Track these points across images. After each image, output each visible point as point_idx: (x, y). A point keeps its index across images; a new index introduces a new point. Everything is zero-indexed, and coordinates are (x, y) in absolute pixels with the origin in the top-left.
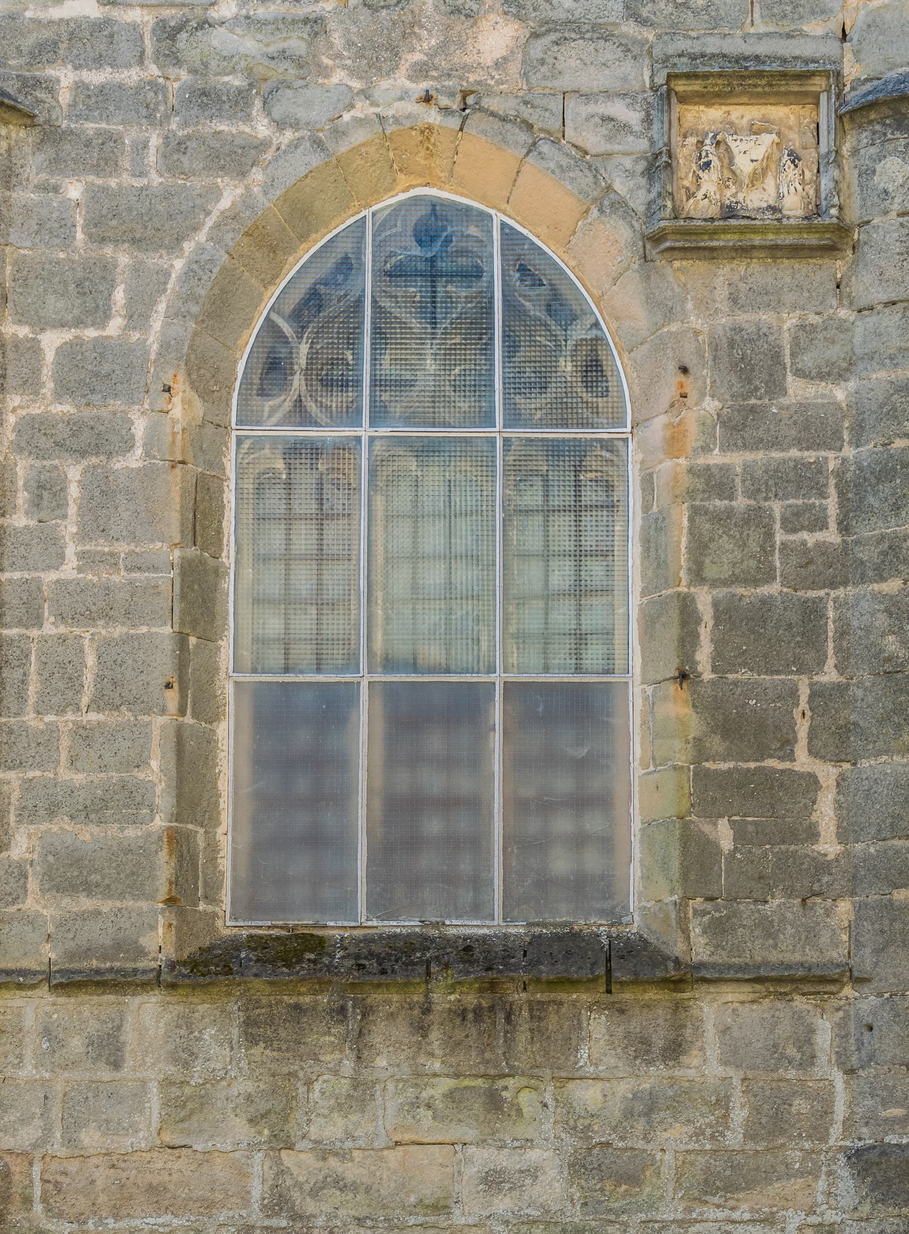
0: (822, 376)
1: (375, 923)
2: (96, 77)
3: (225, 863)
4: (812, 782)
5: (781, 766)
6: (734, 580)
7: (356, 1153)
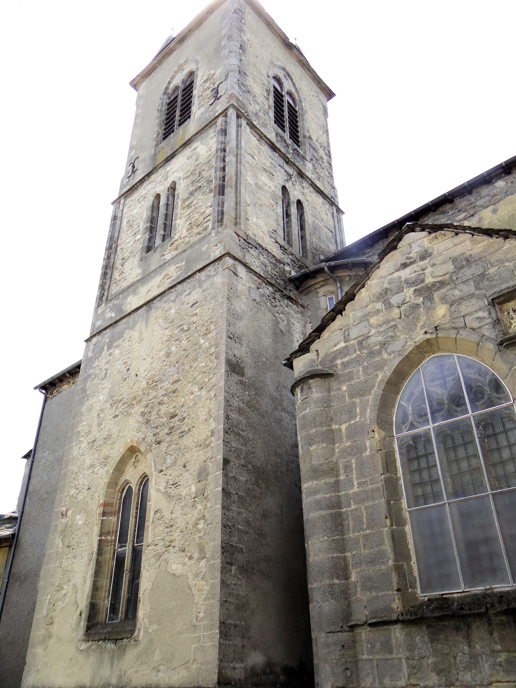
1: (468, 590)
2: (345, 360)
3: (416, 574)
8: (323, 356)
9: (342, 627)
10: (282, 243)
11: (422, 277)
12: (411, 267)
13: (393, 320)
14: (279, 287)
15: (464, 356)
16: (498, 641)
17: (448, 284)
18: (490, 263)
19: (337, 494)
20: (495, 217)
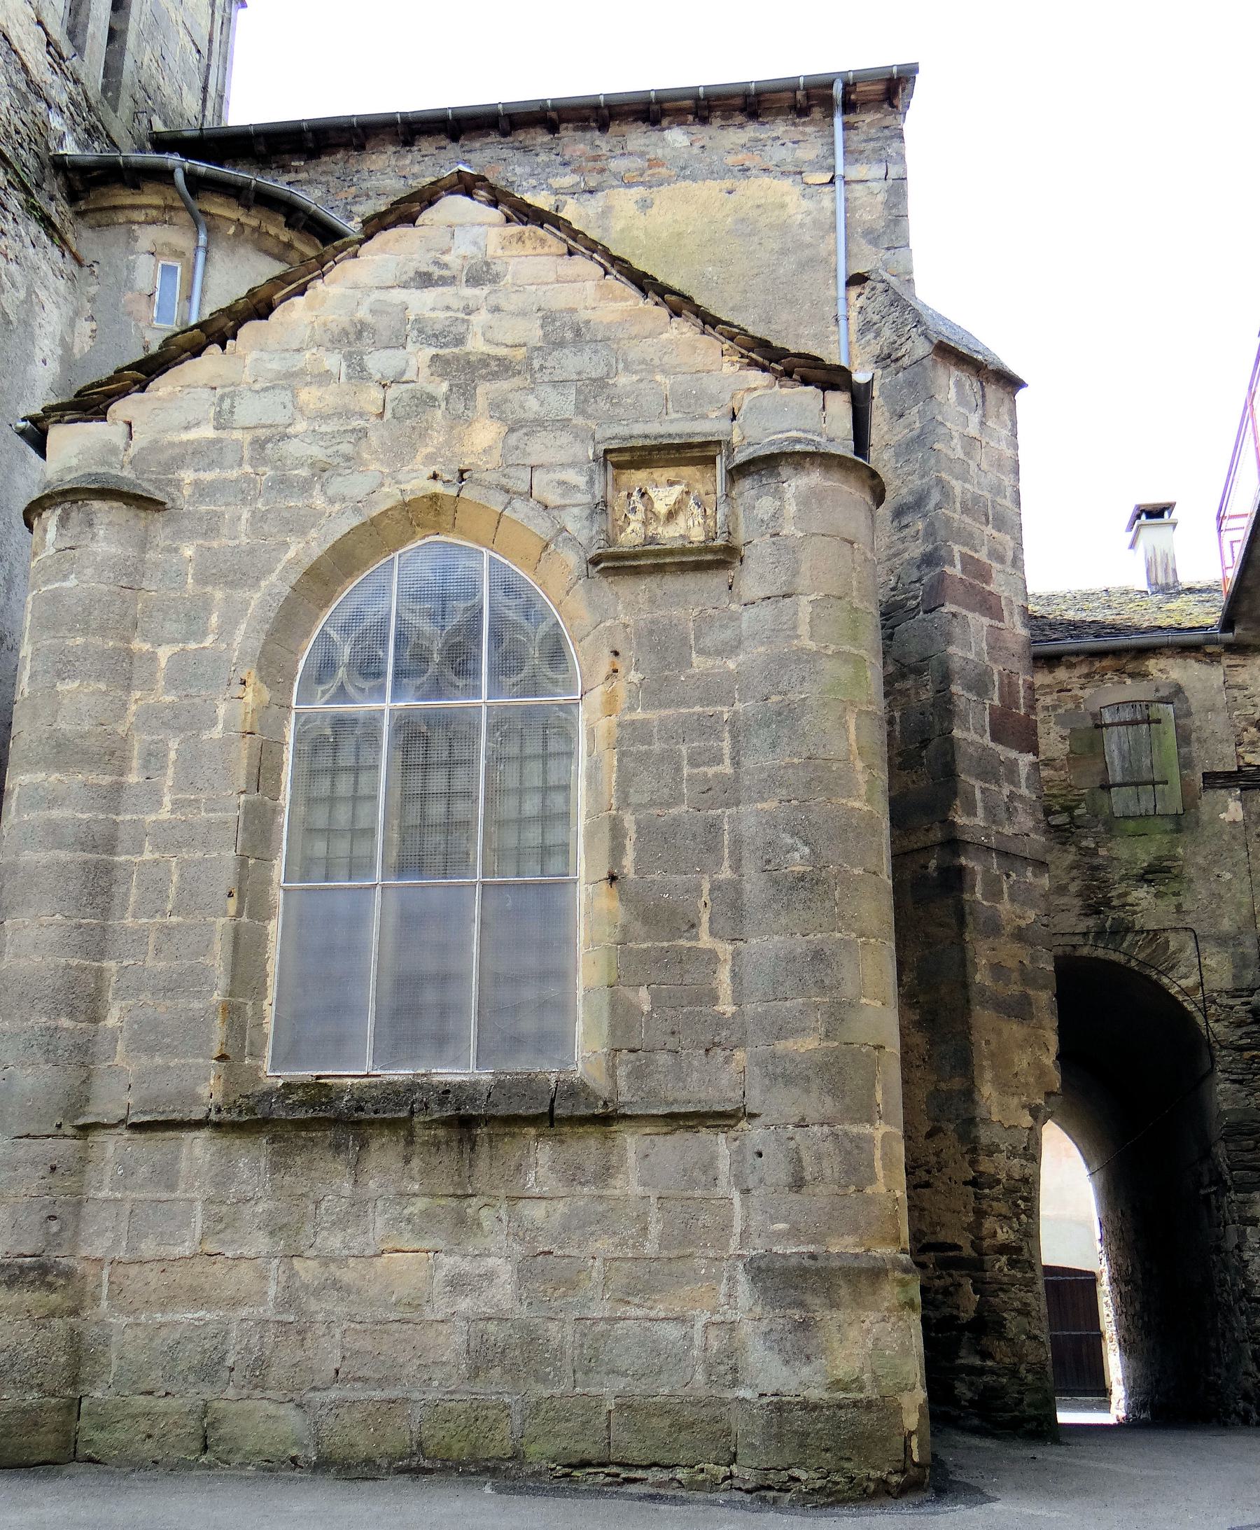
0: (719, 653)
1: (378, 1072)
2: (208, 476)
3: (269, 1028)
4: (712, 958)
5: (689, 944)
6: (652, 803)
7: (351, 1260)
8: (144, 444)
9: (59, 1126)
10: (58, 33)
11: (462, 329)
12: (440, 289)
13: (361, 415)
14: (21, 173)
15: (506, 562)
16: (417, 1176)
17: (519, 373)
18: (625, 361)
19: (110, 816)
20: (641, 221)
